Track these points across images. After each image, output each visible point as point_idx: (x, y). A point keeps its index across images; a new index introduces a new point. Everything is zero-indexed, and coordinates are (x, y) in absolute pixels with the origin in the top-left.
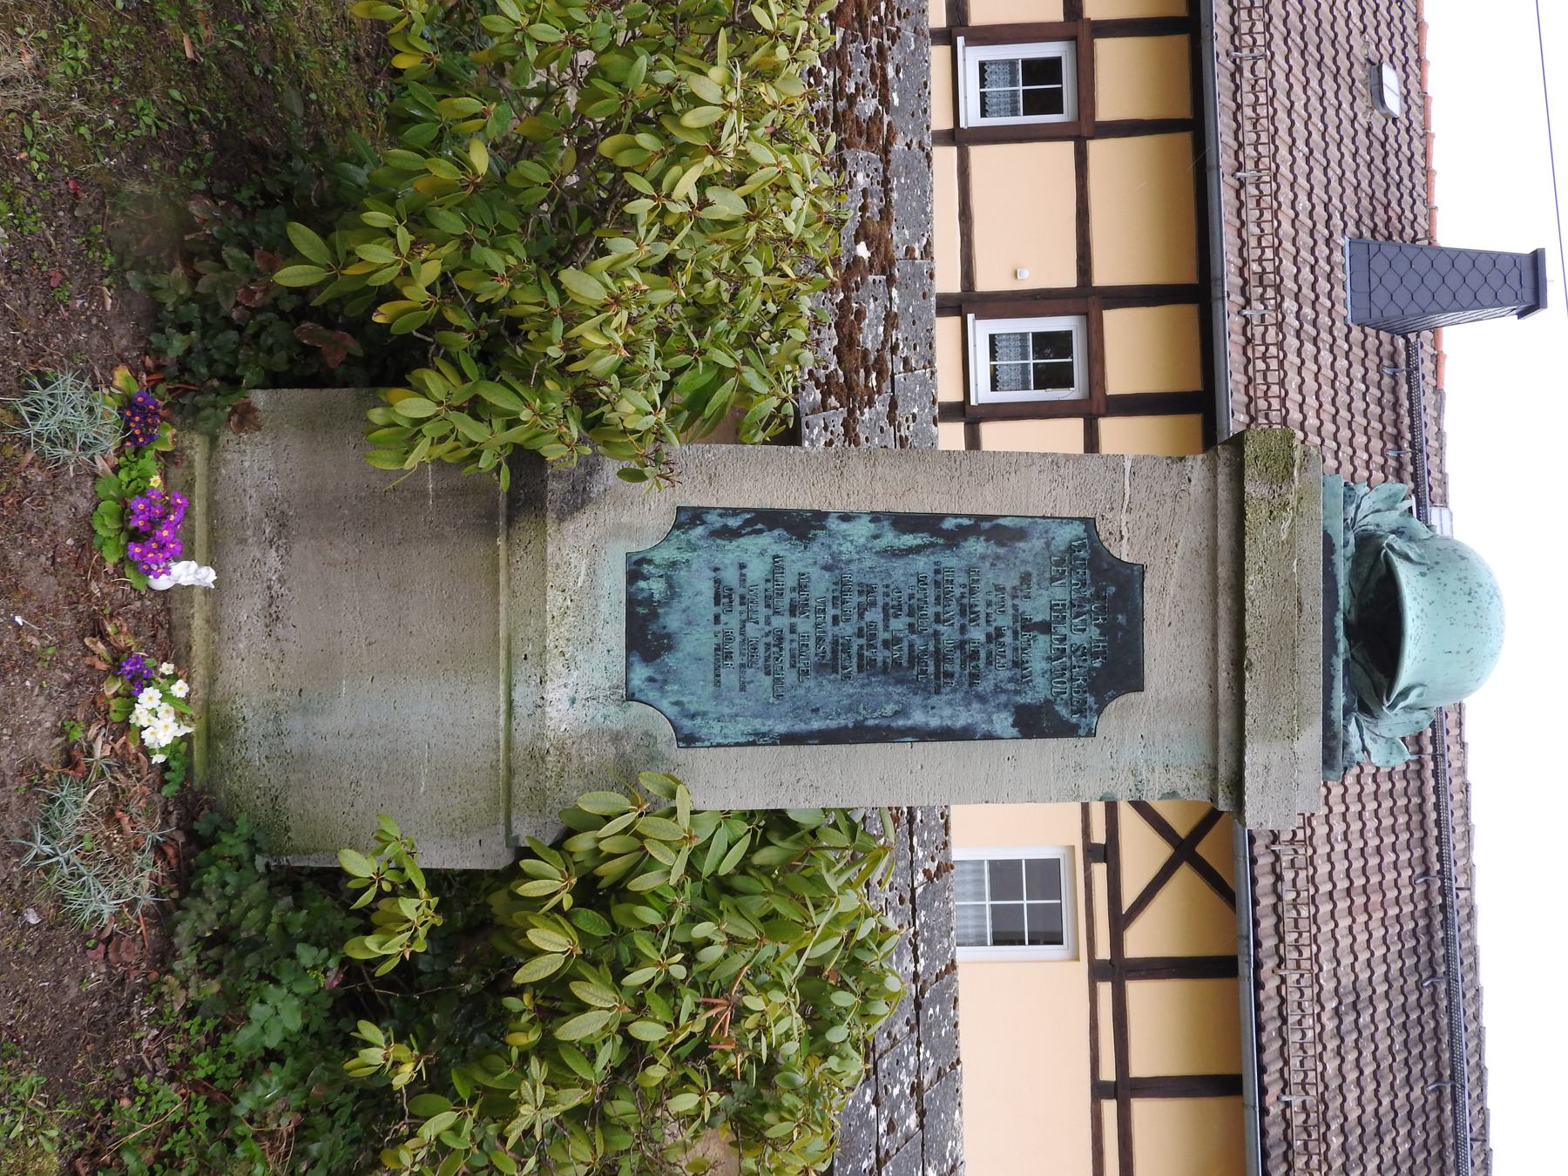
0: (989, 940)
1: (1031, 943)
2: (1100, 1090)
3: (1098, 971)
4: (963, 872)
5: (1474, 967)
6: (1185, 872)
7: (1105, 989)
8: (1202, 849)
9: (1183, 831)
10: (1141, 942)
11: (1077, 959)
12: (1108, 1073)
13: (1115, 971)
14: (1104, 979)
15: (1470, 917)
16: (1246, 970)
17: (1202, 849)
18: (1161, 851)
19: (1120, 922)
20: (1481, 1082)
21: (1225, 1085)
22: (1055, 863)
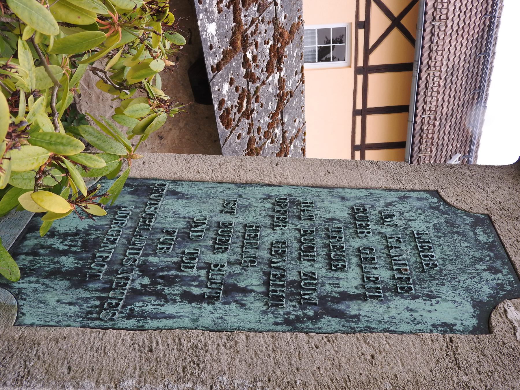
0: (317, 60)
1: (333, 60)
2: (356, 113)
3: (358, 71)
4: (307, 33)
5: (495, 45)
6: (395, 31)
7: (360, 77)
8: (403, 22)
9: (396, 14)
10: (374, 60)
11: (350, 66)
12: (358, 142)
13: (365, 70)
14: (360, 74)
15: (498, 26)
16: (416, 73)
17: (403, 22)
18: (387, 23)
19: (368, 52)
20: (488, 85)
21: (403, 109)
22: (344, 29)
